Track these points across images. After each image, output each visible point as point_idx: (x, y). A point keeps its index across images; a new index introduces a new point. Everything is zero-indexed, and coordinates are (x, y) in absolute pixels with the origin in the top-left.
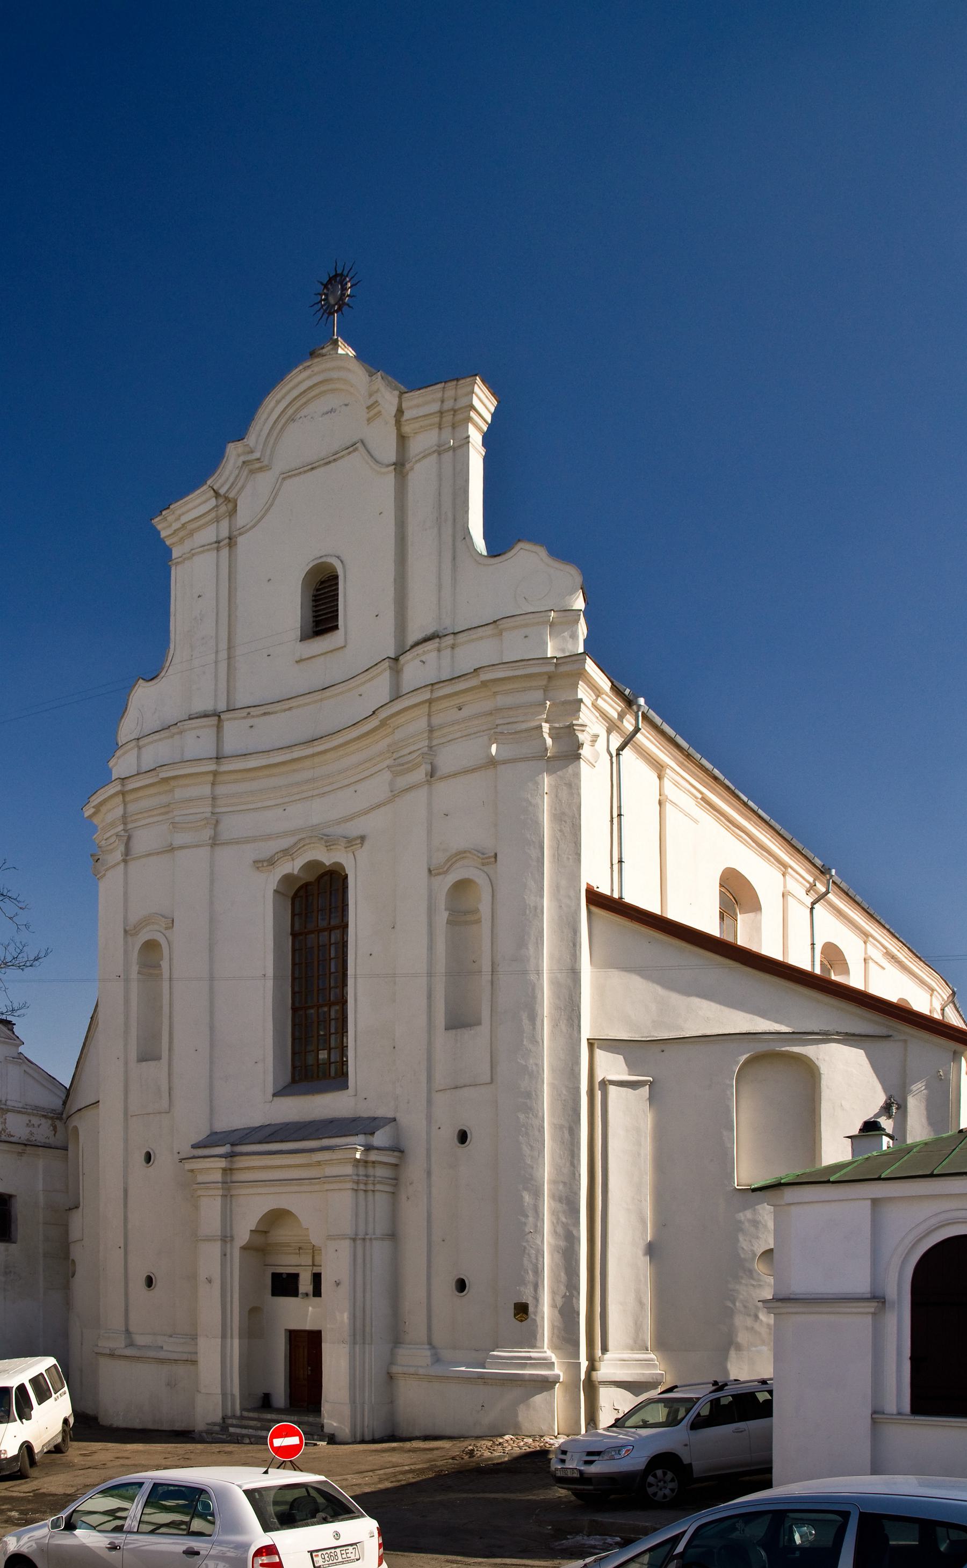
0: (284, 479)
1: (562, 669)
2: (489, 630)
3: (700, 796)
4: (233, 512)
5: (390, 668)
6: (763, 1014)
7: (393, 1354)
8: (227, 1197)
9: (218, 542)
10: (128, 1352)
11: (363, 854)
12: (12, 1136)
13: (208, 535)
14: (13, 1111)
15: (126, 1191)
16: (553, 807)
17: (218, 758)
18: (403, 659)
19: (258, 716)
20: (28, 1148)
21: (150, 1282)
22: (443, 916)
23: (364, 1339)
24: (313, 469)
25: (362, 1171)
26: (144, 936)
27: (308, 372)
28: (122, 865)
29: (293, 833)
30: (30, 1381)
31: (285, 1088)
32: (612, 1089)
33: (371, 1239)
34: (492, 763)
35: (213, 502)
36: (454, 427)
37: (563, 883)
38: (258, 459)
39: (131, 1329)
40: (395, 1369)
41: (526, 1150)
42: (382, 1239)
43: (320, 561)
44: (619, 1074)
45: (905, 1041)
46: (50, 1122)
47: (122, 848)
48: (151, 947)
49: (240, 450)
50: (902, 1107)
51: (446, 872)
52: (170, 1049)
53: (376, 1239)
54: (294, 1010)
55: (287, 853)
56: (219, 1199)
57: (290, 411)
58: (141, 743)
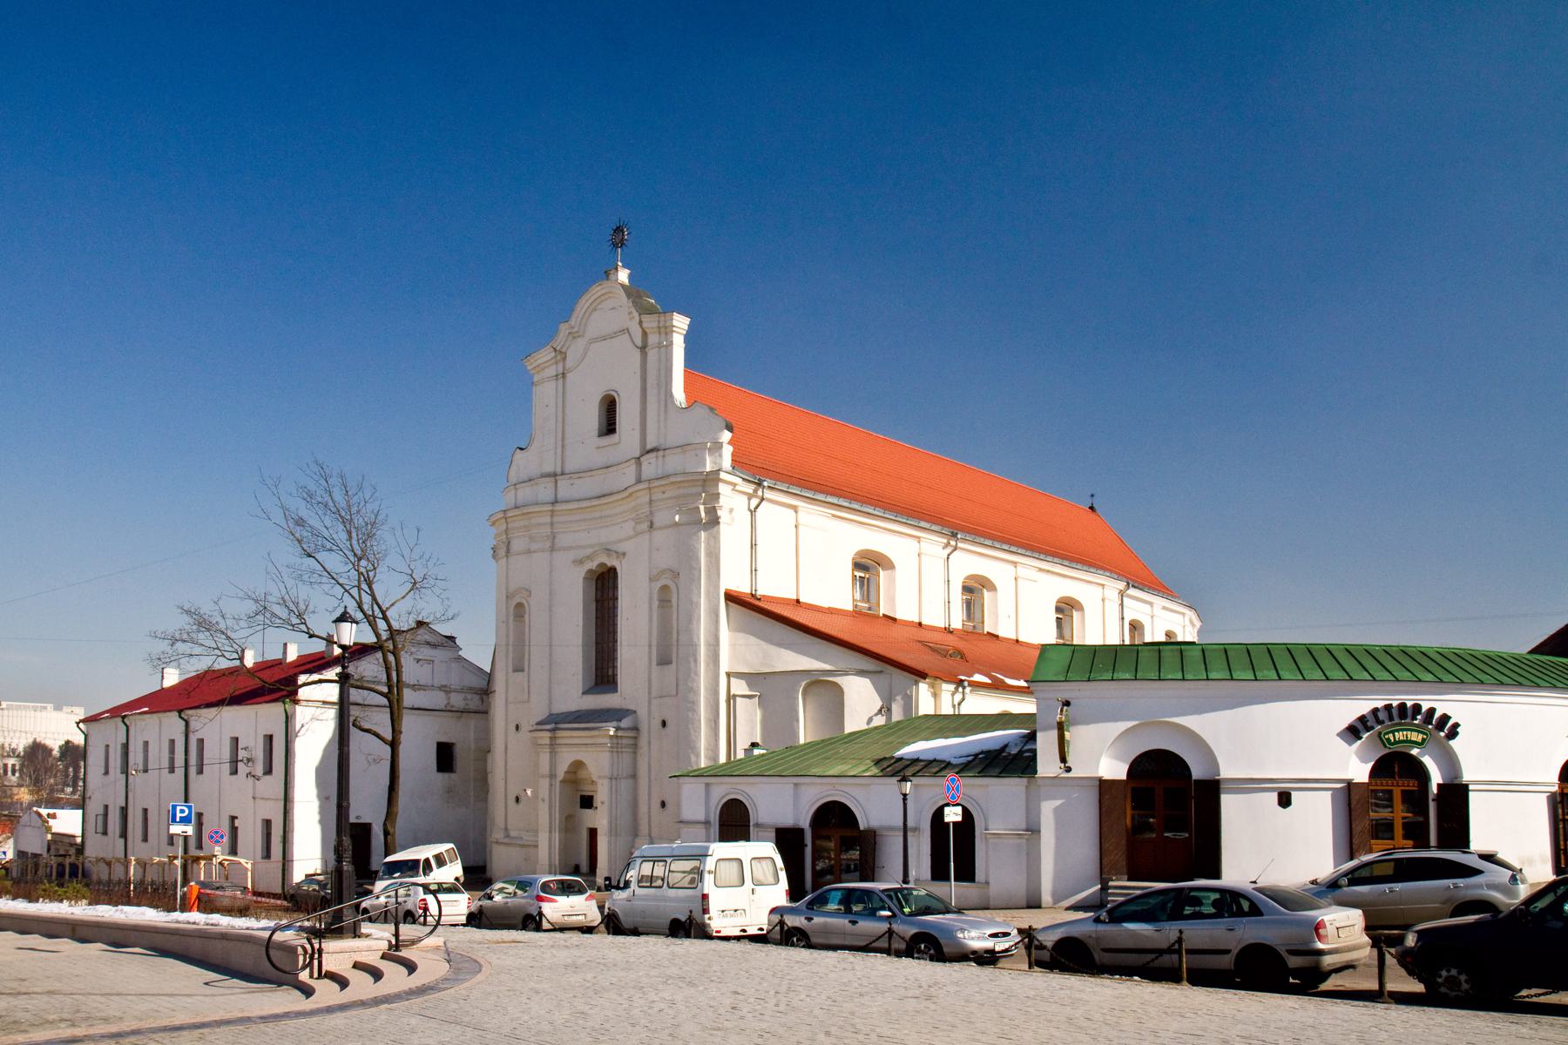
2: (679, 450)
4: (564, 359)
5: (636, 463)
7: (633, 842)
8: (553, 753)
9: (557, 376)
10: (507, 840)
11: (624, 561)
13: (551, 371)
14: (454, 691)
16: (706, 549)
17: (555, 502)
18: (642, 459)
22: (656, 603)
25: (615, 741)
26: (517, 600)
29: (591, 546)
31: (590, 689)
34: (676, 524)
35: (553, 354)
36: (666, 334)
39: (509, 827)
41: (692, 732)
42: (626, 778)
46: (478, 697)
48: (520, 606)
50: (889, 709)
51: (658, 580)
52: (529, 666)
55: (590, 558)
56: (548, 754)
58: (517, 486)
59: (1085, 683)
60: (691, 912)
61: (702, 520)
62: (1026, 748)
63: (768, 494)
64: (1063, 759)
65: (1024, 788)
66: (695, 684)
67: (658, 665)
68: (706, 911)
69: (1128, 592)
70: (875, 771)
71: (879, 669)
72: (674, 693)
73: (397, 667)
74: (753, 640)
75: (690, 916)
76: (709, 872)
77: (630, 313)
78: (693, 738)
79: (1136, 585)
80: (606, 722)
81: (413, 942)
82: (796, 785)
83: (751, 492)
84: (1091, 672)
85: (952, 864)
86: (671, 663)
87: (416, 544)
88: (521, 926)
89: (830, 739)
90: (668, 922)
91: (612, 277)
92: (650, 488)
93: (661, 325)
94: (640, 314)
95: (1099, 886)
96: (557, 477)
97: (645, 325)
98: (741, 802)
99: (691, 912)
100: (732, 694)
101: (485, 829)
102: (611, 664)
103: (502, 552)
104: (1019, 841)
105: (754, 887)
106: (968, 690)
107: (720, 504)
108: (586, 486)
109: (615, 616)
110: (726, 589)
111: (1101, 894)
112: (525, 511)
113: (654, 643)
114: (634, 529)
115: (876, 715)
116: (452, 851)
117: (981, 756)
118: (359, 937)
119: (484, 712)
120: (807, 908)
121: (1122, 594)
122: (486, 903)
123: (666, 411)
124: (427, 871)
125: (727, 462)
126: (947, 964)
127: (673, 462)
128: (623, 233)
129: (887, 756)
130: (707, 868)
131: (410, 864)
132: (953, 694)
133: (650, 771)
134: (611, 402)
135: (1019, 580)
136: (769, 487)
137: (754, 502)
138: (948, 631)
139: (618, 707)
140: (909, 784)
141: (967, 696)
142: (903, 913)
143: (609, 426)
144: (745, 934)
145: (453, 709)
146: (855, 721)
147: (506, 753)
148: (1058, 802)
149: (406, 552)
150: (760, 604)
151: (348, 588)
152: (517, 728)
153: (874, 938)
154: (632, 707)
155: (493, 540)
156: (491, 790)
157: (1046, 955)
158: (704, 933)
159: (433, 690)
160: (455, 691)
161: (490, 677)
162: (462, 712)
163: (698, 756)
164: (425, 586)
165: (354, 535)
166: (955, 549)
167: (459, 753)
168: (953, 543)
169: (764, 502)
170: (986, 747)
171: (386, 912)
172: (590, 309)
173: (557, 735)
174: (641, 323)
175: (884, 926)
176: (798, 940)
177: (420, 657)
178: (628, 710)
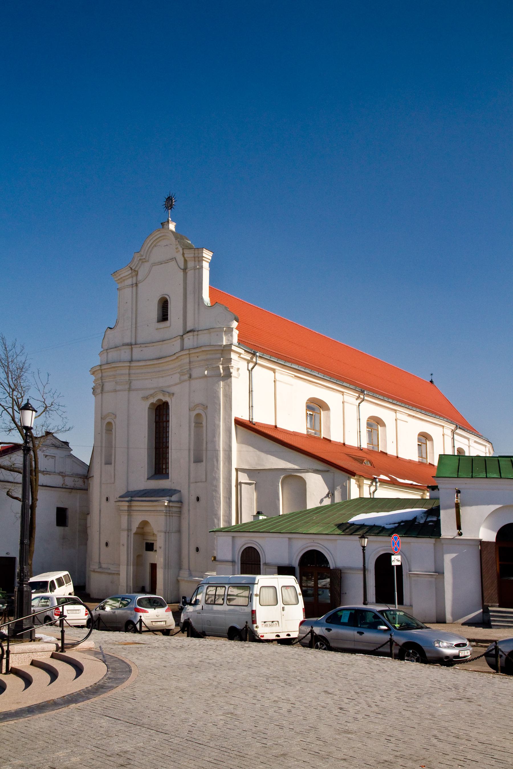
0: (153, 266)
1: (225, 348)
3: (294, 376)
4: (137, 275)
5: (180, 338)
6: (289, 462)
7: (179, 573)
8: (130, 516)
9: (132, 285)
10: (99, 570)
11: (174, 399)
12: (67, 486)
13: (129, 282)
14: (68, 476)
15: (100, 511)
17: (131, 361)
18: (184, 336)
19: (143, 347)
20: (73, 490)
21: (107, 544)
22: (193, 425)
23: (168, 567)
24: (161, 264)
25: (168, 509)
26: (108, 420)
27: (159, 232)
28: (101, 394)
30: (56, 579)
31: (152, 476)
32: (243, 485)
33: (171, 533)
34: (206, 376)
35: (130, 272)
36: (199, 261)
37: (227, 417)
38: (145, 259)
40: (179, 578)
41: (215, 504)
42: (175, 532)
43: (164, 296)
44: (245, 480)
45: (333, 472)
47: (101, 389)
48: (109, 424)
49: (139, 255)
50: (333, 495)
52: (115, 461)
53: (173, 532)
54: (156, 448)
55: (152, 395)
57: (155, 243)
58: (108, 351)
59: (469, 479)
60: (247, 622)
61: (221, 374)
62: (429, 519)
63: (259, 361)
64: (459, 527)
65: (432, 545)
66: (217, 475)
67: (194, 462)
68: (254, 622)
69: (457, 431)
70: (339, 532)
71: (327, 469)
72: (204, 480)
73: (35, 459)
74: (251, 449)
75: (246, 626)
76: (256, 595)
77: (177, 248)
78: (216, 508)
79: (461, 427)
80: (162, 497)
81: (73, 645)
82: (289, 539)
83: (249, 358)
84: (472, 472)
85: (396, 593)
86: (202, 461)
87: (47, 384)
88: (124, 629)
89: (301, 512)
90: (227, 628)
91: (165, 226)
92: (189, 354)
93: (196, 255)
94: (183, 249)
95: (482, 610)
96: (133, 346)
97: (186, 256)
98: (255, 548)
99: (247, 622)
100: (239, 482)
101: (85, 563)
102: (164, 462)
103: (99, 391)
104: (430, 579)
105: (284, 606)
106: (378, 484)
107: (232, 365)
108: (150, 352)
109: (167, 432)
110: (235, 417)
111: (483, 616)
112: (113, 366)
113: (192, 448)
114: (180, 379)
115: (325, 497)
116: (67, 575)
117: (402, 524)
118: (34, 641)
119: (85, 490)
120: (326, 622)
121: (453, 432)
122: (101, 612)
123: (199, 309)
124: (53, 589)
125: (235, 340)
126: (428, 665)
127: (204, 339)
128: (172, 201)
129: (344, 522)
130: (255, 593)
131: (41, 584)
132: (370, 487)
133: (189, 529)
134: (165, 302)
135: (398, 421)
136: (260, 356)
137: (251, 365)
138: (360, 449)
139: (169, 488)
140: (366, 540)
141: (378, 488)
142: (395, 627)
143: (164, 316)
144: (279, 638)
145: (67, 487)
146: (312, 503)
147: (462, 443)
148: (454, 555)
149: (41, 388)
150: (255, 427)
151: (6, 408)
152: (107, 499)
153: (380, 645)
154: (178, 488)
155: (93, 383)
156: (89, 537)
157: (501, 661)
158: (254, 638)
159: (54, 474)
160: (68, 476)
161: (89, 468)
162: (72, 489)
163: (219, 519)
164: (52, 409)
165: (10, 375)
166: (363, 400)
167: (70, 514)
168: (362, 396)
169: (257, 367)
170: (405, 518)
171: (34, 617)
172: (153, 246)
173: (133, 505)
174: (183, 254)
175: (386, 637)
176: (320, 644)
177: (47, 454)
178: (175, 490)
